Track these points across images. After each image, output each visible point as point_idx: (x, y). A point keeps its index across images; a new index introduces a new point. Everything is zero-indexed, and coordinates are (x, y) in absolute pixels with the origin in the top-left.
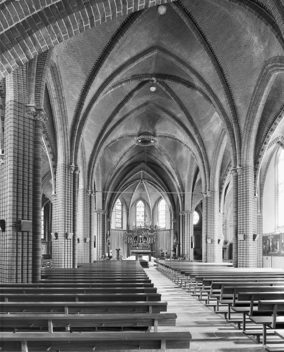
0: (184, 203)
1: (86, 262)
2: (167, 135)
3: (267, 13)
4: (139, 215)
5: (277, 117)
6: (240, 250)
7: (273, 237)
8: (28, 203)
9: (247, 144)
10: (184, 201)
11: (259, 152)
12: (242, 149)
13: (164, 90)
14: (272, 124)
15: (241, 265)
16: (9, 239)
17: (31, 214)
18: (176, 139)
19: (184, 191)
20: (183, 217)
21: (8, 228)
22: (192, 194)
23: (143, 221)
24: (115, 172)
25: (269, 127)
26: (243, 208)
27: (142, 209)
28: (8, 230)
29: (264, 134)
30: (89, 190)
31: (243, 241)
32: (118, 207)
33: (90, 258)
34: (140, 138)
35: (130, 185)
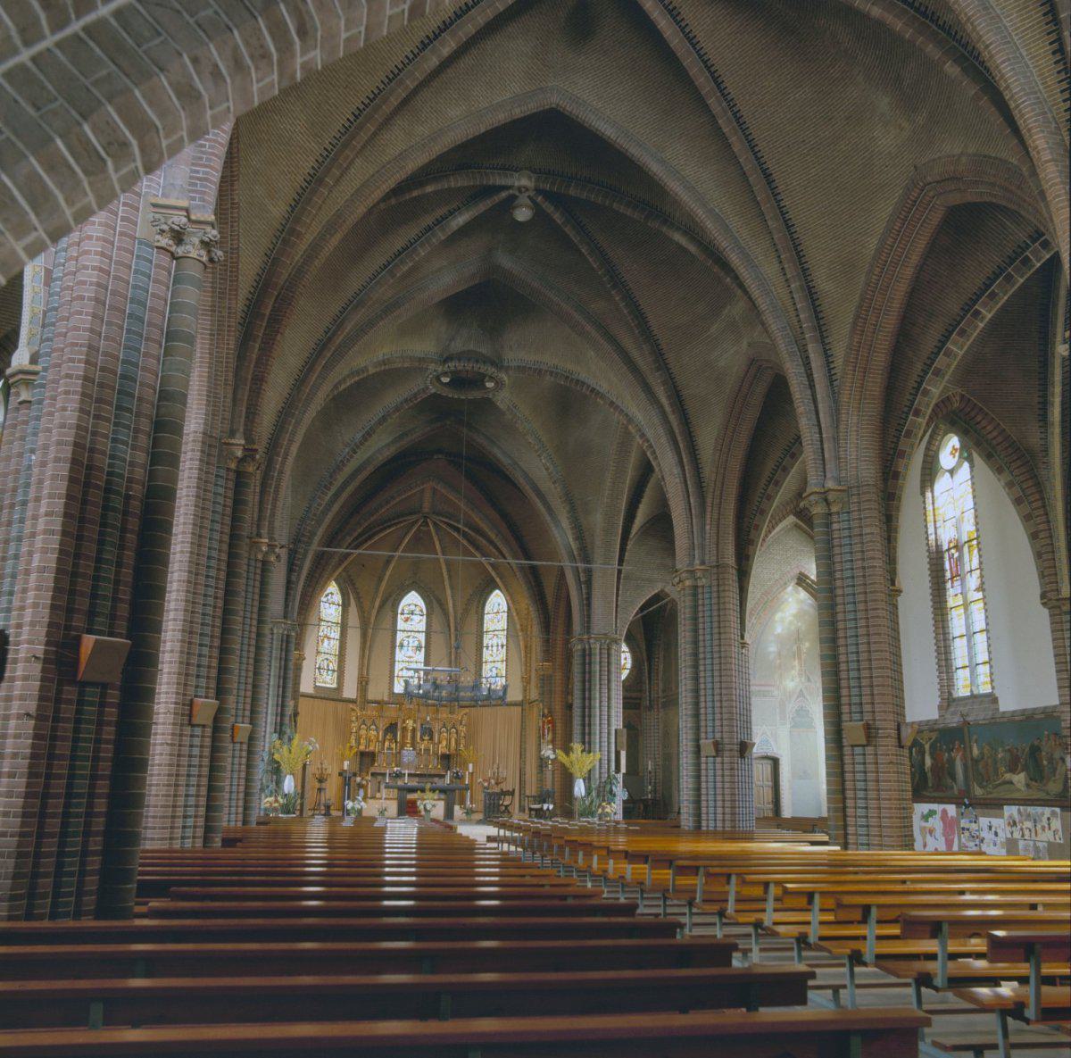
0: (589, 605)
1: (229, 821)
2: (545, 368)
3: (940, 31)
4: (405, 643)
5: (951, 333)
6: (854, 781)
7: (934, 736)
8: (119, 565)
9: (859, 411)
10: (589, 599)
11: (898, 440)
12: (842, 427)
13: (558, 221)
14: (938, 353)
15: (863, 840)
16: (19, 717)
17: (124, 610)
18: (578, 381)
19: (587, 559)
20: (586, 655)
21: (20, 665)
22: (620, 572)
23: (422, 666)
24: (340, 479)
25: (925, 364)
26: (856, 628)
27: (419, 623)
28: (19, 673)
29: (912, 383)
30: (263, 540)
31: (864, 746)
32: (329, 611)
33: (246, 808)
34: (446, 369)
35: (381, 531)
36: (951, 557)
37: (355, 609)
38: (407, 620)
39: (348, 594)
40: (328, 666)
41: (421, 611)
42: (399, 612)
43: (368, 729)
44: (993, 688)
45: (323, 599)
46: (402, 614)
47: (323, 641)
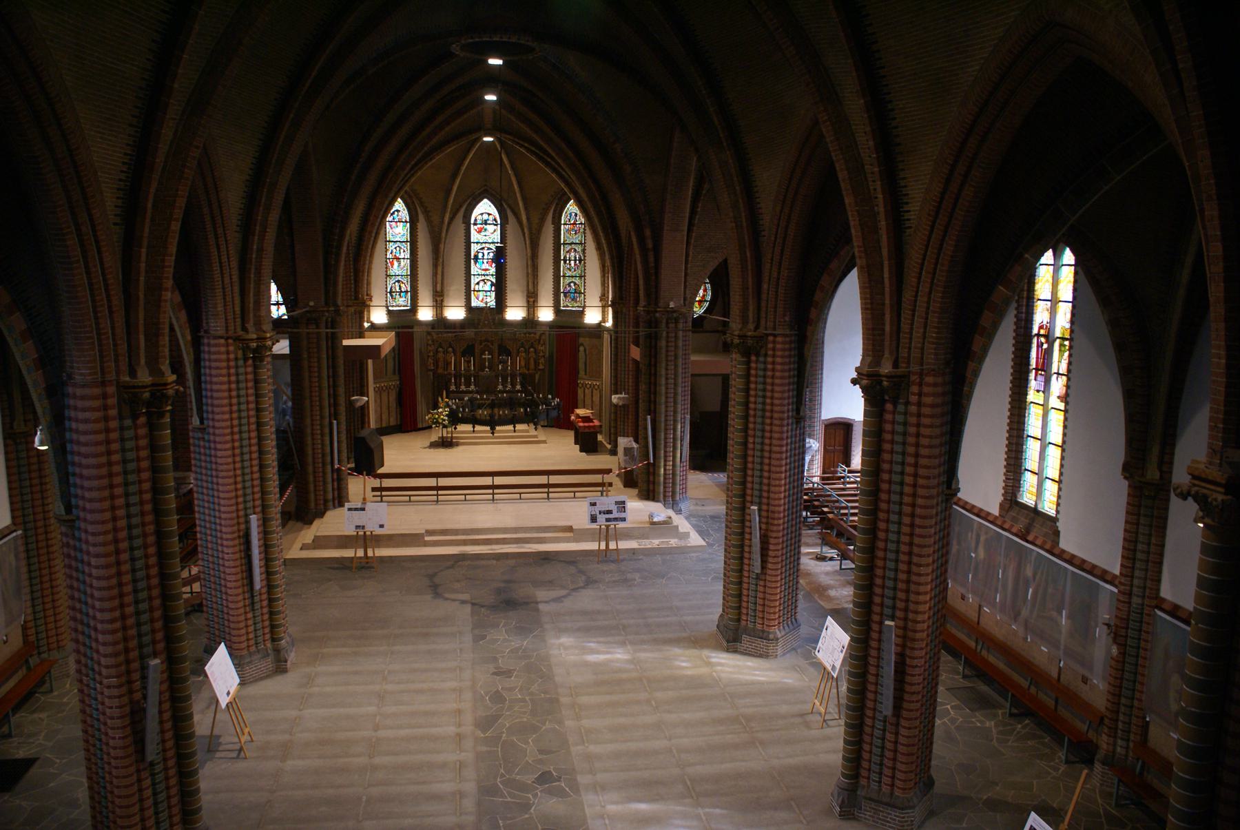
4: (480, 255)
36: (1040, 345)
37: (424, 220)
38: (479, 231)
39: (416, 209)
40: (400, 288)
41: (495, 220)
42: (472, 221)
43: (446, 352)
44: (1057, 512)
45: (389, 218)
46: (475, 224)
47: (392, 264)
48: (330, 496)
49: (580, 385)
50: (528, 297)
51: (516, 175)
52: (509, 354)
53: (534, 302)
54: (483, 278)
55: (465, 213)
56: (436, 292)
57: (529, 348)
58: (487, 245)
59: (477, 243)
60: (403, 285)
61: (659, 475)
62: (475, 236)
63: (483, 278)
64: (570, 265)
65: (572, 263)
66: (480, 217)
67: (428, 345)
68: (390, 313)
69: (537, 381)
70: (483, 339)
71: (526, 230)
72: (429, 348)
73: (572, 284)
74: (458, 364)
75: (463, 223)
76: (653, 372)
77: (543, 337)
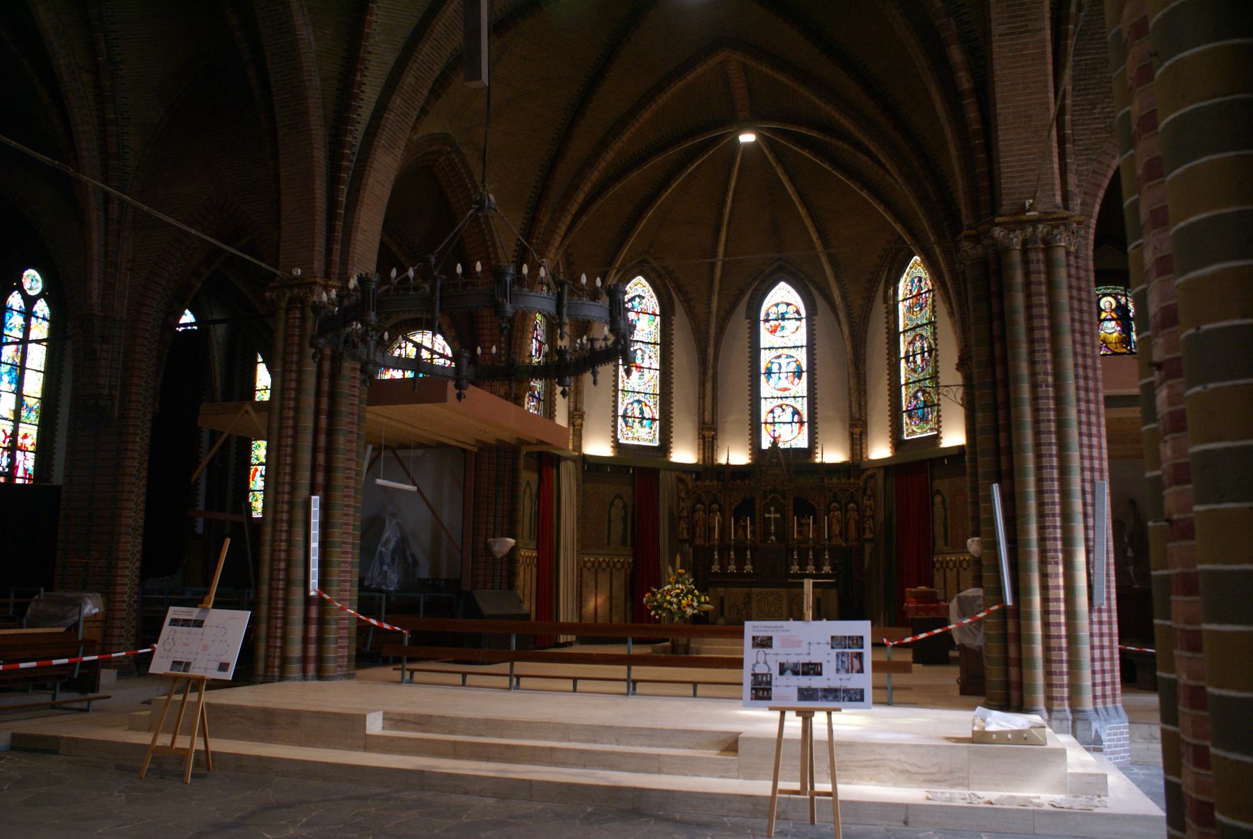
4: (775, 368)
38: (773, 331)
39: (670, 296)
40: (642, 412)
41: (798, 312)
42: (762, 316)
46: (767, 321)
48: (296, 650)
49: (938, 565)
50: (852, 426)
51: (815, 220)
52: (812, 511)
53: (861, 434)
54: (780, 402)
55: (749, 303)
56: (704, 423)
57: (847, 504)
58: (786, 351)
59: (770, 349)
60: (646, 409)
61: (1030, 639)
62: (766, 339)
63: (780, 402)
64: (915, 362)
65: (918, 358)
66: (774, 309)
67: (679, 498)
68: (617, 446)
69: (866, 566)
70: (769, 488)
71: (842, 315)
72: (682, 504)
73: (919, 394)
74: (724, 529)
75: (747, 318)
76: (999, 376)
77: (871, 483)
